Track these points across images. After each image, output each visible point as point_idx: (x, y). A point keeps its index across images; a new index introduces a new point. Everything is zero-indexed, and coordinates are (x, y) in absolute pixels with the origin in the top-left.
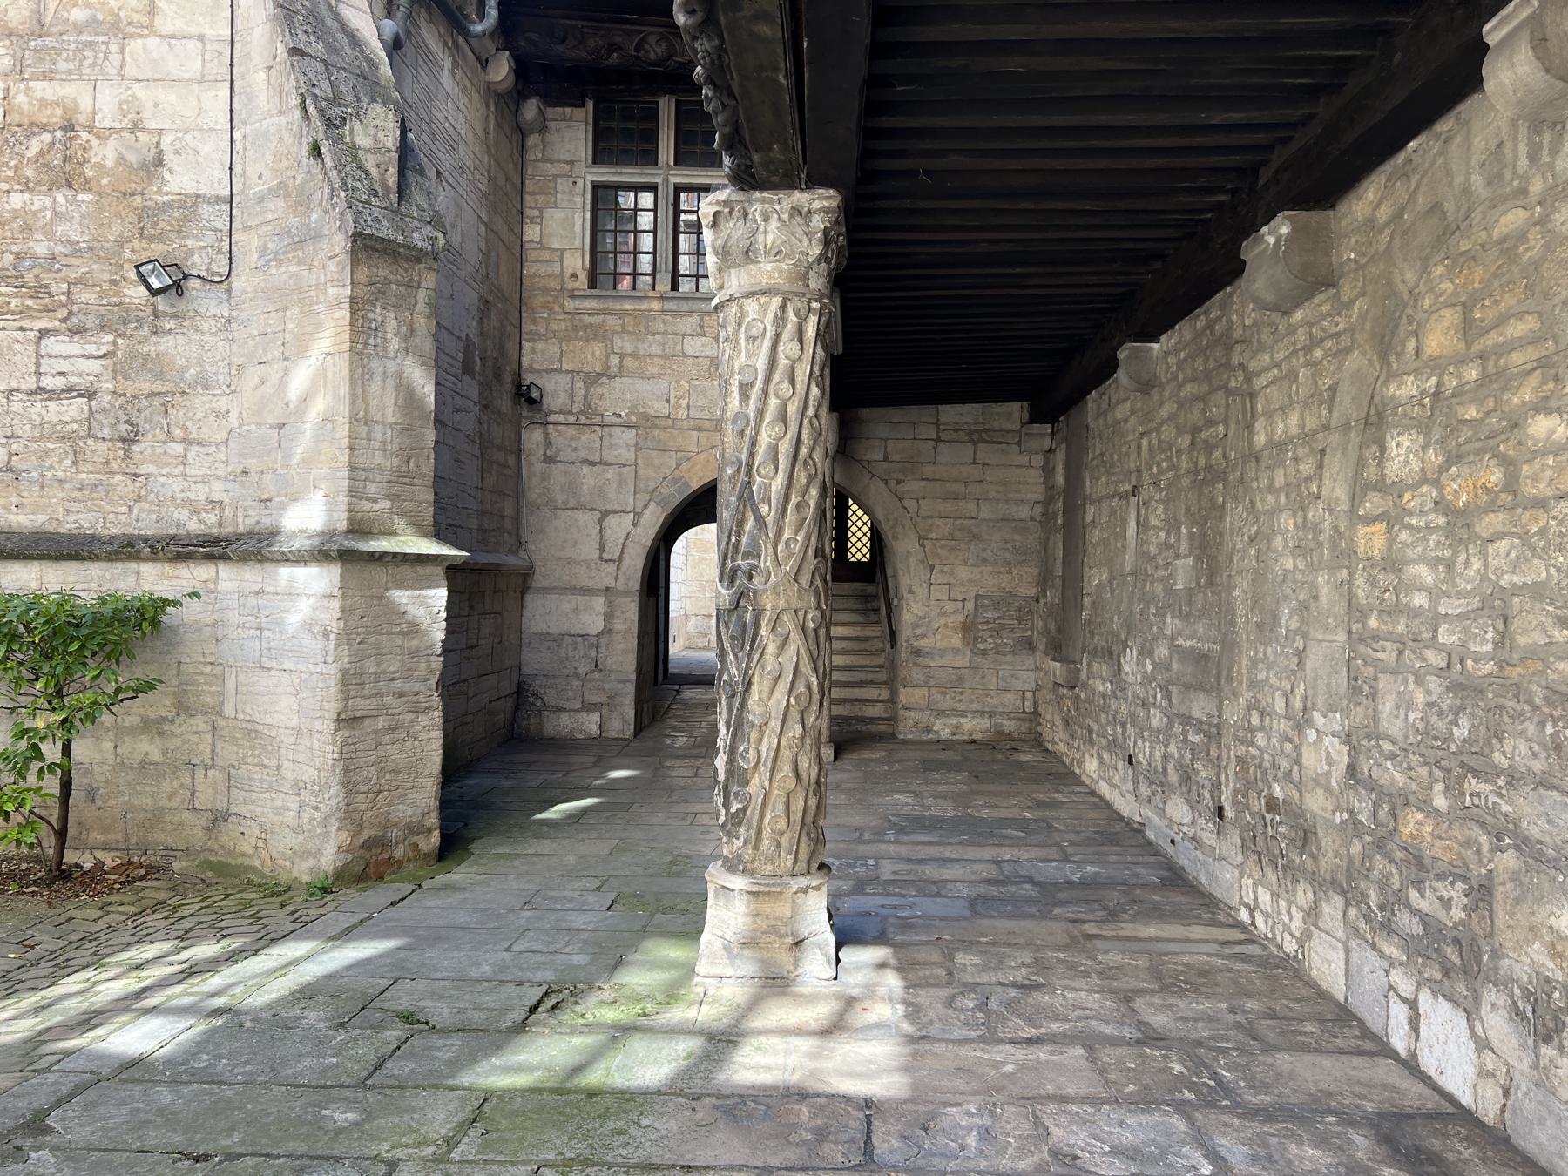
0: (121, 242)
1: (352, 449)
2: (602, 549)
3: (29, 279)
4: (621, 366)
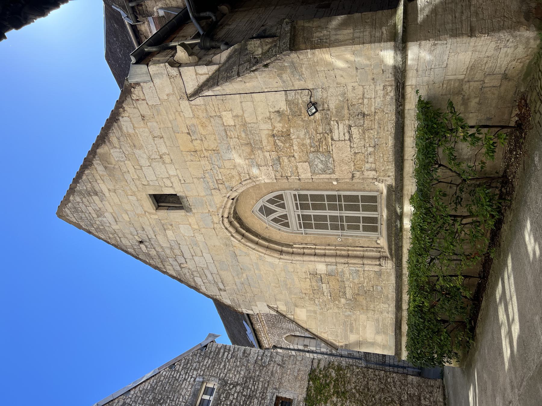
3: (317, 144)
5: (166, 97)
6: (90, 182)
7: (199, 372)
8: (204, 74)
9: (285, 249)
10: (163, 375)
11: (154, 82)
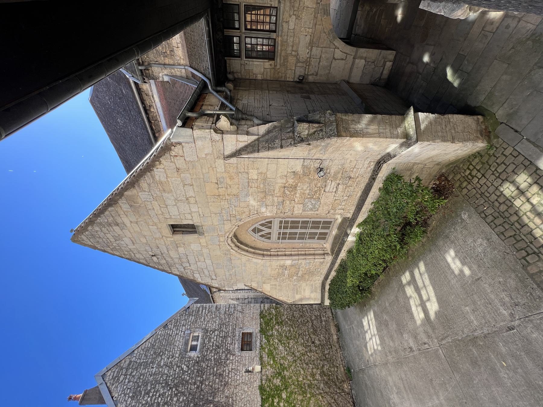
0: (309, 179)
1: (387, 138)
2: (342, 59)
3: (313, 193)
4: (295, 51)
5: (204, 156)
6: (112, 217)
7: (187, 327)
8: (244, 142)
9: (265, 253)
10: (159, 334)
11: (196, 143)
